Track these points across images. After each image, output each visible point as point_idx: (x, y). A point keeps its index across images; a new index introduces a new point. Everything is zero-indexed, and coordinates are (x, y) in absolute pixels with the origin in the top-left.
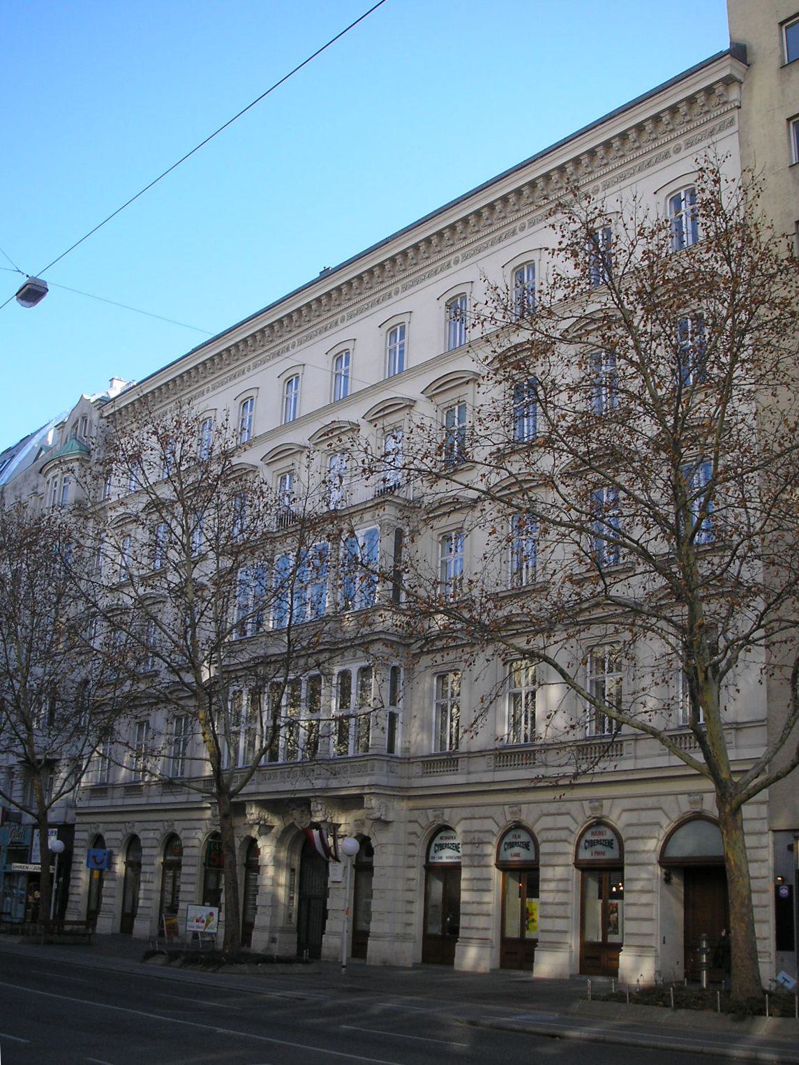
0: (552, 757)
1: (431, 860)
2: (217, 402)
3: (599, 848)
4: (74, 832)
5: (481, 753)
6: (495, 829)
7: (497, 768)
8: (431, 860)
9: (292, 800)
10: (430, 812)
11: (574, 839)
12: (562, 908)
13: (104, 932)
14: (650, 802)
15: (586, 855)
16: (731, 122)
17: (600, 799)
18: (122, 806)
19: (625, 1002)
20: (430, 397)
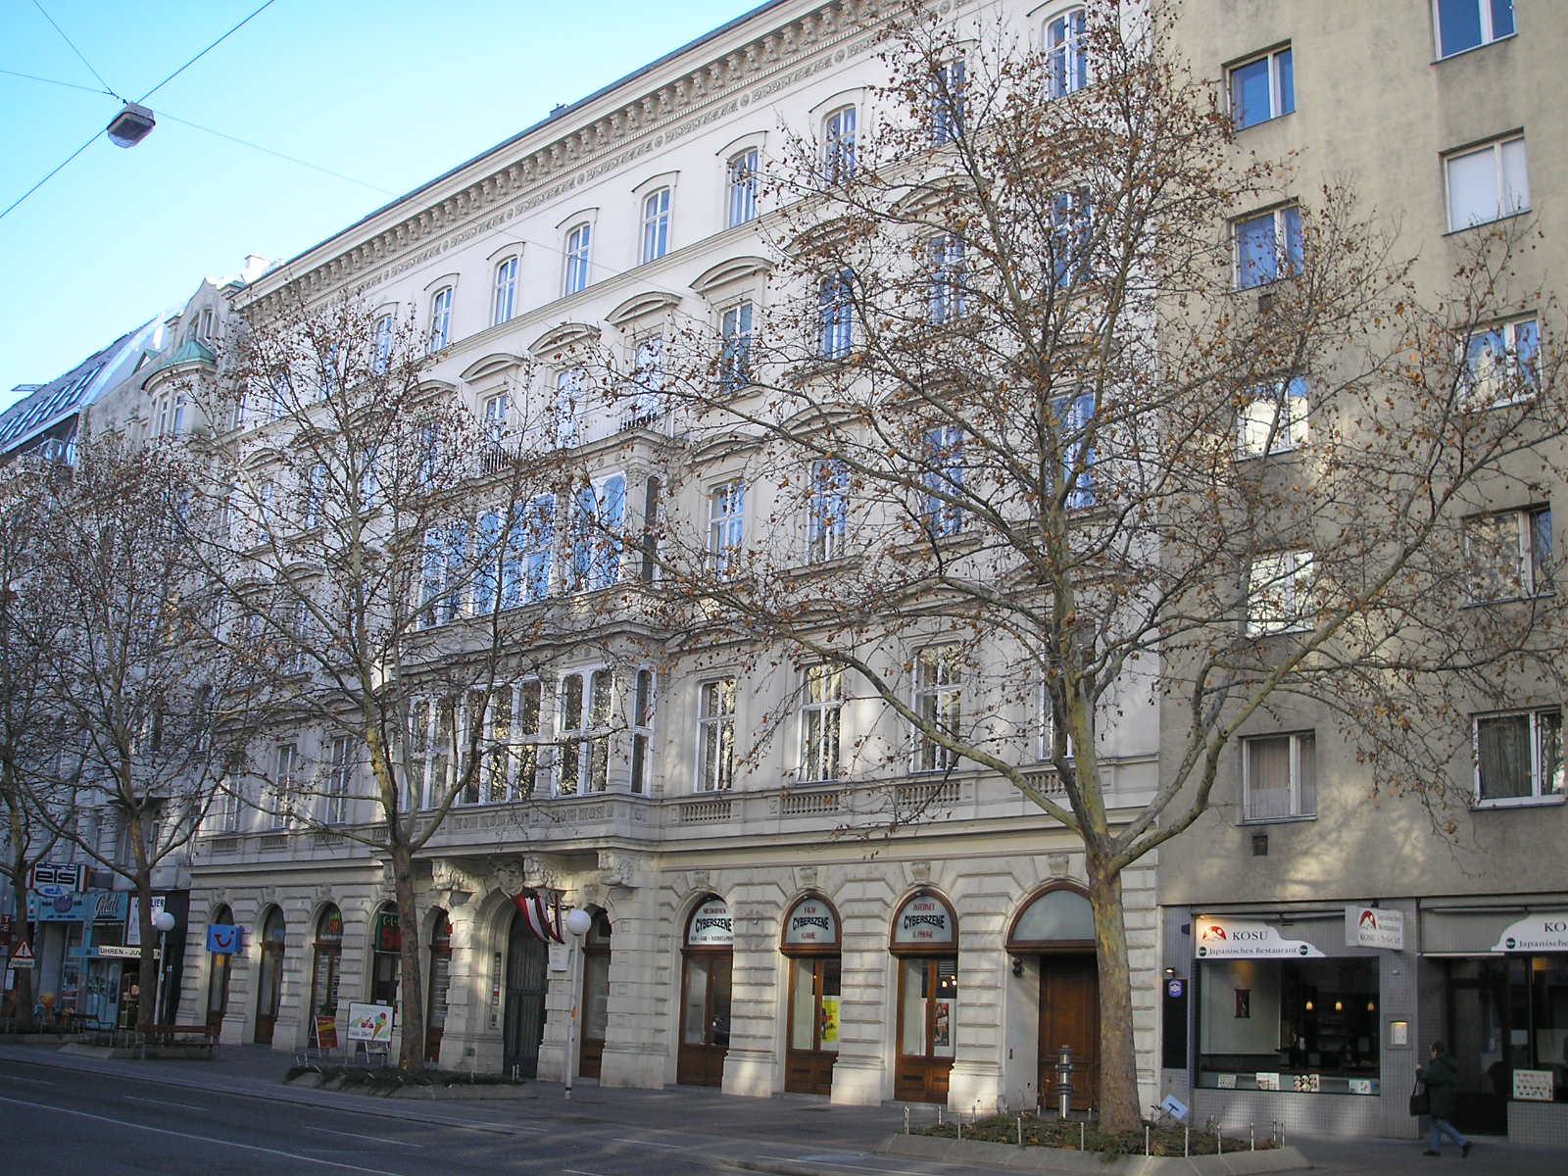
1: (691, 942)
2: (400, 292)
3: (924, 927)
5: (763, 794)
6: (781, 899)
7: (785, 815)
8: (691, 942)
14: (996, 865)
15: (906, 937)
17: (927, 860)
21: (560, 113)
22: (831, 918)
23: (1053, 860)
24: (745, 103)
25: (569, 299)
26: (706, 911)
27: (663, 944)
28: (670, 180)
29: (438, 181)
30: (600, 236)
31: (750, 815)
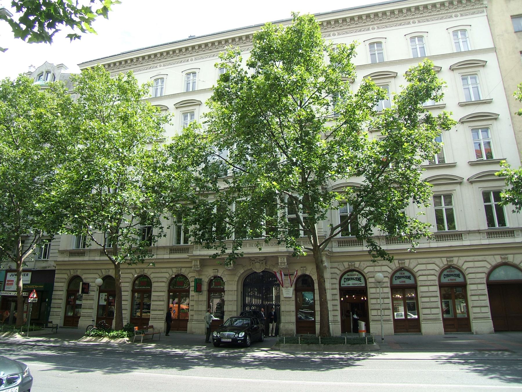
0: (160, 252)
1: (342, 286)
2: (142, 78)
3: (452, 278)
4: (55, 274)
5: (164, 248)
6: (338, 272)
7: (170, 253)
8: (342, 286)
9: (256, 258)
10: (103, 271)
11: (338, 277)
12: (475, 305)
13: (335, 335)
14: (480, 258)
15: (445, 280)
16: (483, 12)
17: (404, 260)
18: (169, 258)
19: (318, 343)
20: (177, 108)
21: (192, 38)
22: (410, 275)
23: (502, 257)
24: (192, 60)
25: (187, 93)
26: (348, 275)
27: (334, 286)
28: (165, 77)
29: (158, 46)
30: (200, 76)
31: (158, 253)
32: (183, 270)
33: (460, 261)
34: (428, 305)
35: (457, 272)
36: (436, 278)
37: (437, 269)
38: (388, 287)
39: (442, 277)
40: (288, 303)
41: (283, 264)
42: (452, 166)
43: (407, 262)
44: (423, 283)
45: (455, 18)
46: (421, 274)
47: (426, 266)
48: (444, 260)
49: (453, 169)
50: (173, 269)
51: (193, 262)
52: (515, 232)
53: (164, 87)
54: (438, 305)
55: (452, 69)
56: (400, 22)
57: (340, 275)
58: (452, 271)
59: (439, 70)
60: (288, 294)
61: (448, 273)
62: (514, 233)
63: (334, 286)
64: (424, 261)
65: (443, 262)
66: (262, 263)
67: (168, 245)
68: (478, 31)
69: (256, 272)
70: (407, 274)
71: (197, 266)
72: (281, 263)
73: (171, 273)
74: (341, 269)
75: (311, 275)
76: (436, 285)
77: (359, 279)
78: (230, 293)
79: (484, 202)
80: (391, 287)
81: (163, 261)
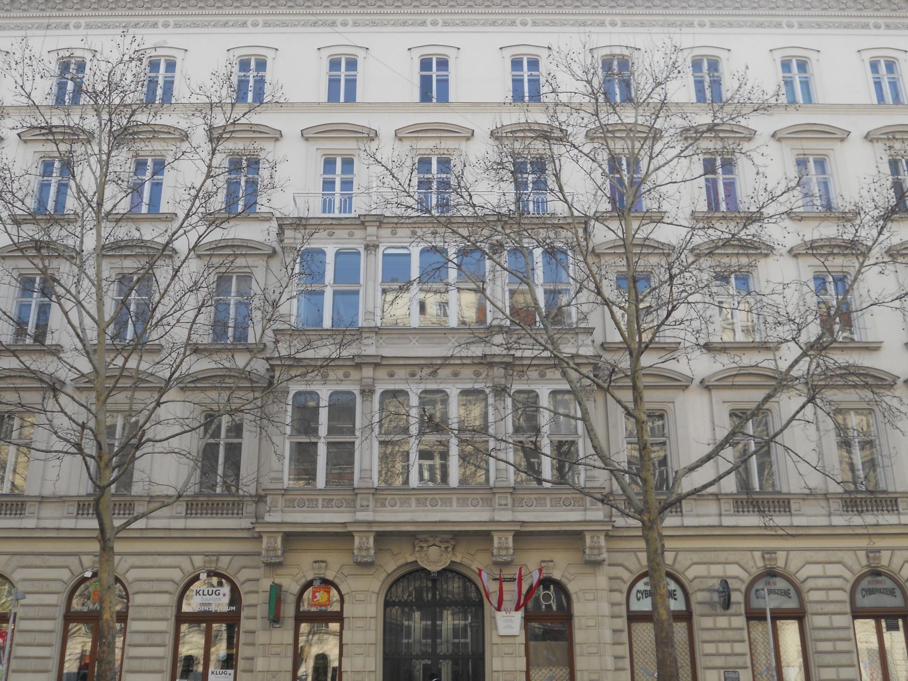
0: (48, 511)
9: (434, 534)
22: (894, 586)
27: (617, 610)
31: (43, 514)
32: (224, 561)
33: (895, 560)
34: (829, 659)
35: (889, 584)
36: (845, 596)
37: (848, 575)
38: (740, 615)
39: (858, 596)
40: (507, 650)
41: (503, 552)
42: (873, 348)
43: (781, 555)
44: (818, 608)
45: (875, 31)
46: (813, 586)
47: (824, 569)
48: (862, 555)
49: (875, 355)
50: (194, 557)
51: (265, 540)
52: (899, 500)
53: (870, 75)
54: (745, 662)
55: (869, 138)
56: (313, 18)
57: (629, 584)
58: (878, 582)
59: (750, 136)
60: (510, 627)
61: (871, 587)
62: (897, 505)
63: (617, 610)
64: (821, 556)
65: (859, 563)
66: (447, 548)
67: (73, 492)
68: (841, 64)
69: (424, 569)
70: (889, 584)
71: (275, 550)
72: (592, 548)
73: (77, 569)
74: (632, 567)
75: (564, 580)
76: (845, 614)
77: (786, 593)
78: (360, 623)
79: (241, 444)
80: (746, 613)
81: (168, 535)
